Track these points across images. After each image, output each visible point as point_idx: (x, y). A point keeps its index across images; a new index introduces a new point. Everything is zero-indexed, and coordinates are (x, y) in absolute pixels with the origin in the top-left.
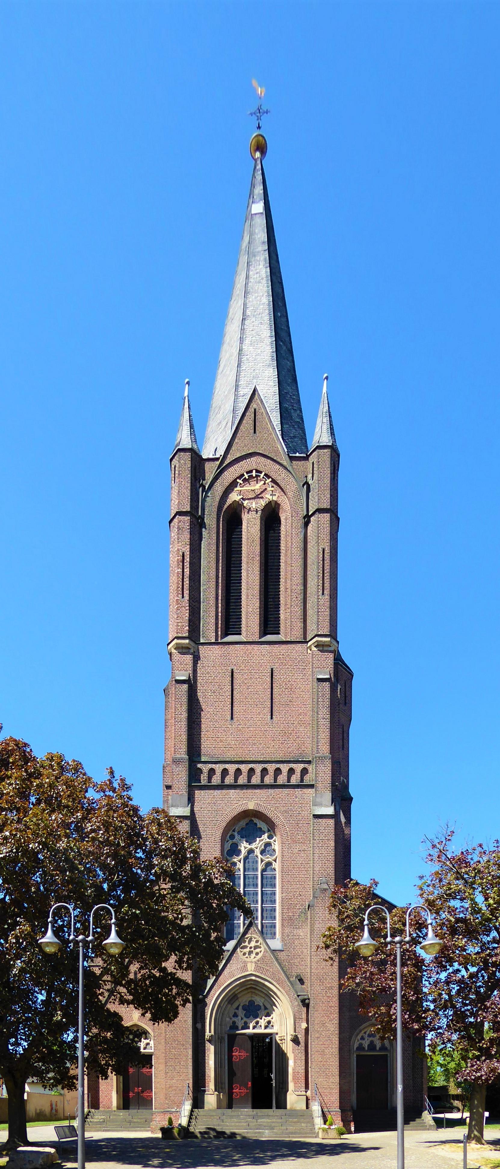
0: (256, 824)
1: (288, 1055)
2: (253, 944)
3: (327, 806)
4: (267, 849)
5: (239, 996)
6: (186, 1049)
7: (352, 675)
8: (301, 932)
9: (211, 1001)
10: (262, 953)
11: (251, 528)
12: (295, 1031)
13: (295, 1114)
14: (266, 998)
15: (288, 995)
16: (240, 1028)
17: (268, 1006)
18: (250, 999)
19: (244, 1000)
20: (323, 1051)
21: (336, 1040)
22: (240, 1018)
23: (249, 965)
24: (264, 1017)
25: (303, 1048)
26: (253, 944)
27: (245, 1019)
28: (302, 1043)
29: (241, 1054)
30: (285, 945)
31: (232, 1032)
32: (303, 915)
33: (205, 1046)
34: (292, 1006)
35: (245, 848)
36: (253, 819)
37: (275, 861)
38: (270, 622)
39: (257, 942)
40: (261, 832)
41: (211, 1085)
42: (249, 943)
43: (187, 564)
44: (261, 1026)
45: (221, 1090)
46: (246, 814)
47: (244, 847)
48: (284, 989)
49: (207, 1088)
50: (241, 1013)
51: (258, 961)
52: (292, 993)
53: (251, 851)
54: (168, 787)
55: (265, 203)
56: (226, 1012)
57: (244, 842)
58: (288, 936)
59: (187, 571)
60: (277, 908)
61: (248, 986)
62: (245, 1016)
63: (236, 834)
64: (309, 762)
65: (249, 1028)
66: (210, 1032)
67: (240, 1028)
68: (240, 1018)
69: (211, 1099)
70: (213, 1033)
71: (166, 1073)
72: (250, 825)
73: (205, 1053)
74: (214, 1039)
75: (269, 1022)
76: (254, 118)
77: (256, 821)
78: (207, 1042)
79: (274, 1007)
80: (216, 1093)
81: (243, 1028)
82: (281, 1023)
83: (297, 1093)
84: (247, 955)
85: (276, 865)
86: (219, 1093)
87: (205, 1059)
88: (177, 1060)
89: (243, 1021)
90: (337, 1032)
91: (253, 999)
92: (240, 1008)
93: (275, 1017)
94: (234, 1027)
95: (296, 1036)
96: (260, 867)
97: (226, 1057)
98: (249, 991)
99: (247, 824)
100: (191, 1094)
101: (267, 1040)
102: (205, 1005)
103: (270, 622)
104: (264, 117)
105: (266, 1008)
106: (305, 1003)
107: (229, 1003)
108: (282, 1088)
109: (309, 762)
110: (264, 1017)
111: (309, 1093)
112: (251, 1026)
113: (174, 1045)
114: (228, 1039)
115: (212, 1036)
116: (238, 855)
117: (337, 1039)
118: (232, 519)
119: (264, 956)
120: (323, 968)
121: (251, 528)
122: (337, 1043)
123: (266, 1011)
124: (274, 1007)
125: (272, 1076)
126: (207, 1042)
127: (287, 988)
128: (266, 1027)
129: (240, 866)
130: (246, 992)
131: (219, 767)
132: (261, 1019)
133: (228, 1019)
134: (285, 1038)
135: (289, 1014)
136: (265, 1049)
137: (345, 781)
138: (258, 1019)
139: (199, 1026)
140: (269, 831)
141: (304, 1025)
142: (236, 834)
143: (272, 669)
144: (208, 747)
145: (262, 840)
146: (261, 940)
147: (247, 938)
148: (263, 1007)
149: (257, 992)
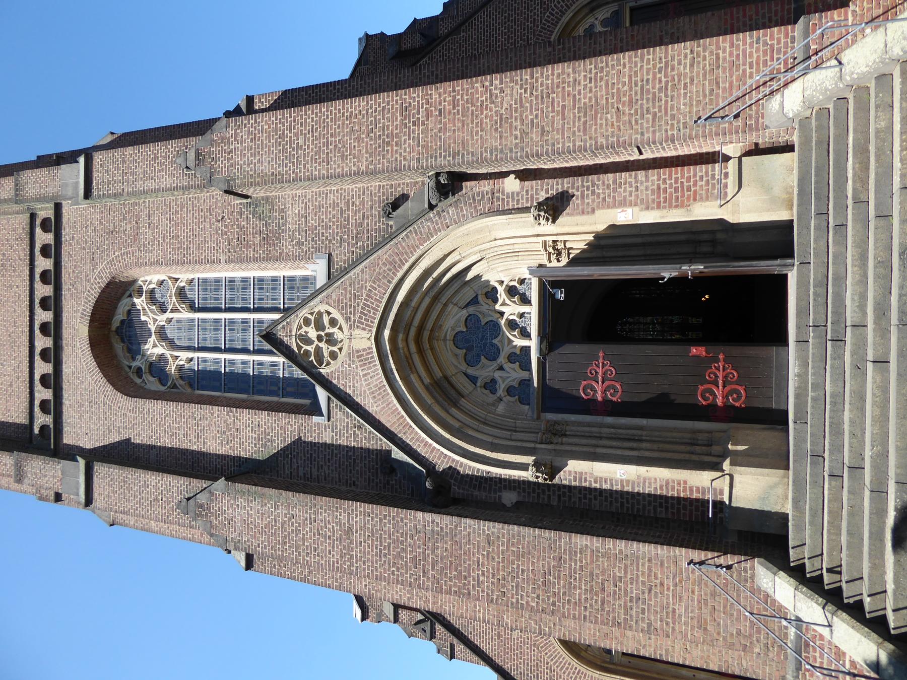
0: (122, 322)
1: (601, 227)
2: (313, 333)
5: (439, 374)
6: (572, 553)
8: (292, 213)
9: (443, 458)
10: (331, 309)
12: (526, 210)
13: (816, 187)
14: (444, 300)
15: (437, 231)
16: (524, 375)
17: (467, 294)
18: (450, 344)
19: (451, 360)
20: (585, 110)
21: (549, 76)
22: (497, 375)
24: (498, 307)
25: (579, 181)
26: (313, 333)
27: (502, 359)
28: (566, 184)
29: (601, 375)
30: (318, 250)
31: (534, 399)
32: (259, 210)
33: (570, 488)
34: (458, 223)
35: (155, 346)
36: (114, 328)
39: (307, 322)
40: (132, 311)
41: (698, 482)
42: (309, 341)
44: (522, 315)
45: (716, 449)
47: (153, 349)
48: (414, 248)
49: (710, 497)
50: (485, 371)
51: (348, 319)
52: (425, 225)
53: (162, 333)
54: (58, 497)
56: (482, 413)
57: (146, 347)
58: (300, 244)
60: (289, 273)
61: (413, 348)
64: (33, 216)
65: (527, 349)
66: (523, 467)
67: (524, 375)
68: (497, 375)
69: (750, 488)
70: (529, 460)
73: (590, 490)
74: (548, 458)
75: (511, 291)
78: (556, 481)
79: (470, 275)
80: (726, 465)
81: (527, 367)
82: (509, 251)
83: (731, 189)
84: (335, 349)
85: (184, 276)
86: (724, 457)
87: (611, 492)
88: (610, 589)
89: (508, 366)
90: (526, 74)
91: (450, 336)
92: (471, 371)
93: (496, 274)
94: (521, 390)
95: (540, 206)
96: (186, 315)
97: (609, 420)
98: (426, 346)
99: (123, 341)
100: (730, 559)
101: (560, 295)
102: (452, 472)
105: (474, 301)
106: (450, 184)
107: (455, 404)
108: (713, 242)
109: (33, 216)
110: (498, 307)
111: (732, 149)
112: (520, 342)
113: (559, 587)
114: (557, 415)
115: (537, 464)
116: (166, 360)
117: (548, 70)
119: (338, 304)
120: (358, 140)
122: (558, 68)
123: (481, 299)
124: (470, 275)
125: (667, 275)
126: (556, 481)
127: (413, 239)
128: (525, 300)
129: (184, 355)
130: (429, 353)
131: (39, 392)
132: (502, 314)
133: (501, 408)
134: (549, 239)
135: (479, 231)
136: (585, 307)
138: (503, 322)
139: (509, 498)
141: (511, 184)
142: (134, 364)
145: (144, 309)
146: (304, 313)
147: (299, 348)
148: (472, 309)
149: (430, 325)
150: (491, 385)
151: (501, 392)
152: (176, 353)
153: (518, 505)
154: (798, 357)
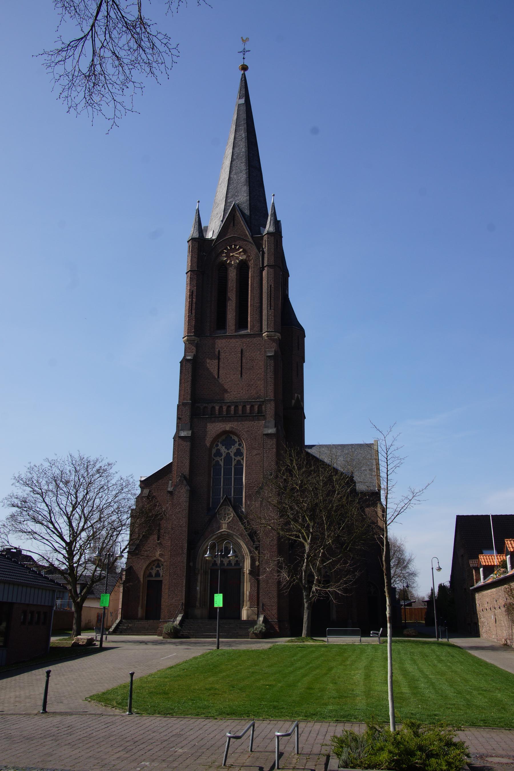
0: (231, 437)
3: (248, 616)
4: (239, 453)
11: (232, 274)
37: (221, 460)
38: (242, 323)
40: (234, 442)
43: (194, 297)
46: (225, 432)
51: (229, 522)
55: (245, 98)
59: (194, 300)
63: (219, 444)
71: (169, 595)
72: (227, 438)
76: (242, 54)
103: (242, 323)
104: (247, 54)
118: (224, 267)
121: (232, 274)
129: (222, 463)
137: (299, 396)
139: (191, 564)
140: (239, 441)
142: (219, 444)
143: (242, 350)
144: (217, 361)
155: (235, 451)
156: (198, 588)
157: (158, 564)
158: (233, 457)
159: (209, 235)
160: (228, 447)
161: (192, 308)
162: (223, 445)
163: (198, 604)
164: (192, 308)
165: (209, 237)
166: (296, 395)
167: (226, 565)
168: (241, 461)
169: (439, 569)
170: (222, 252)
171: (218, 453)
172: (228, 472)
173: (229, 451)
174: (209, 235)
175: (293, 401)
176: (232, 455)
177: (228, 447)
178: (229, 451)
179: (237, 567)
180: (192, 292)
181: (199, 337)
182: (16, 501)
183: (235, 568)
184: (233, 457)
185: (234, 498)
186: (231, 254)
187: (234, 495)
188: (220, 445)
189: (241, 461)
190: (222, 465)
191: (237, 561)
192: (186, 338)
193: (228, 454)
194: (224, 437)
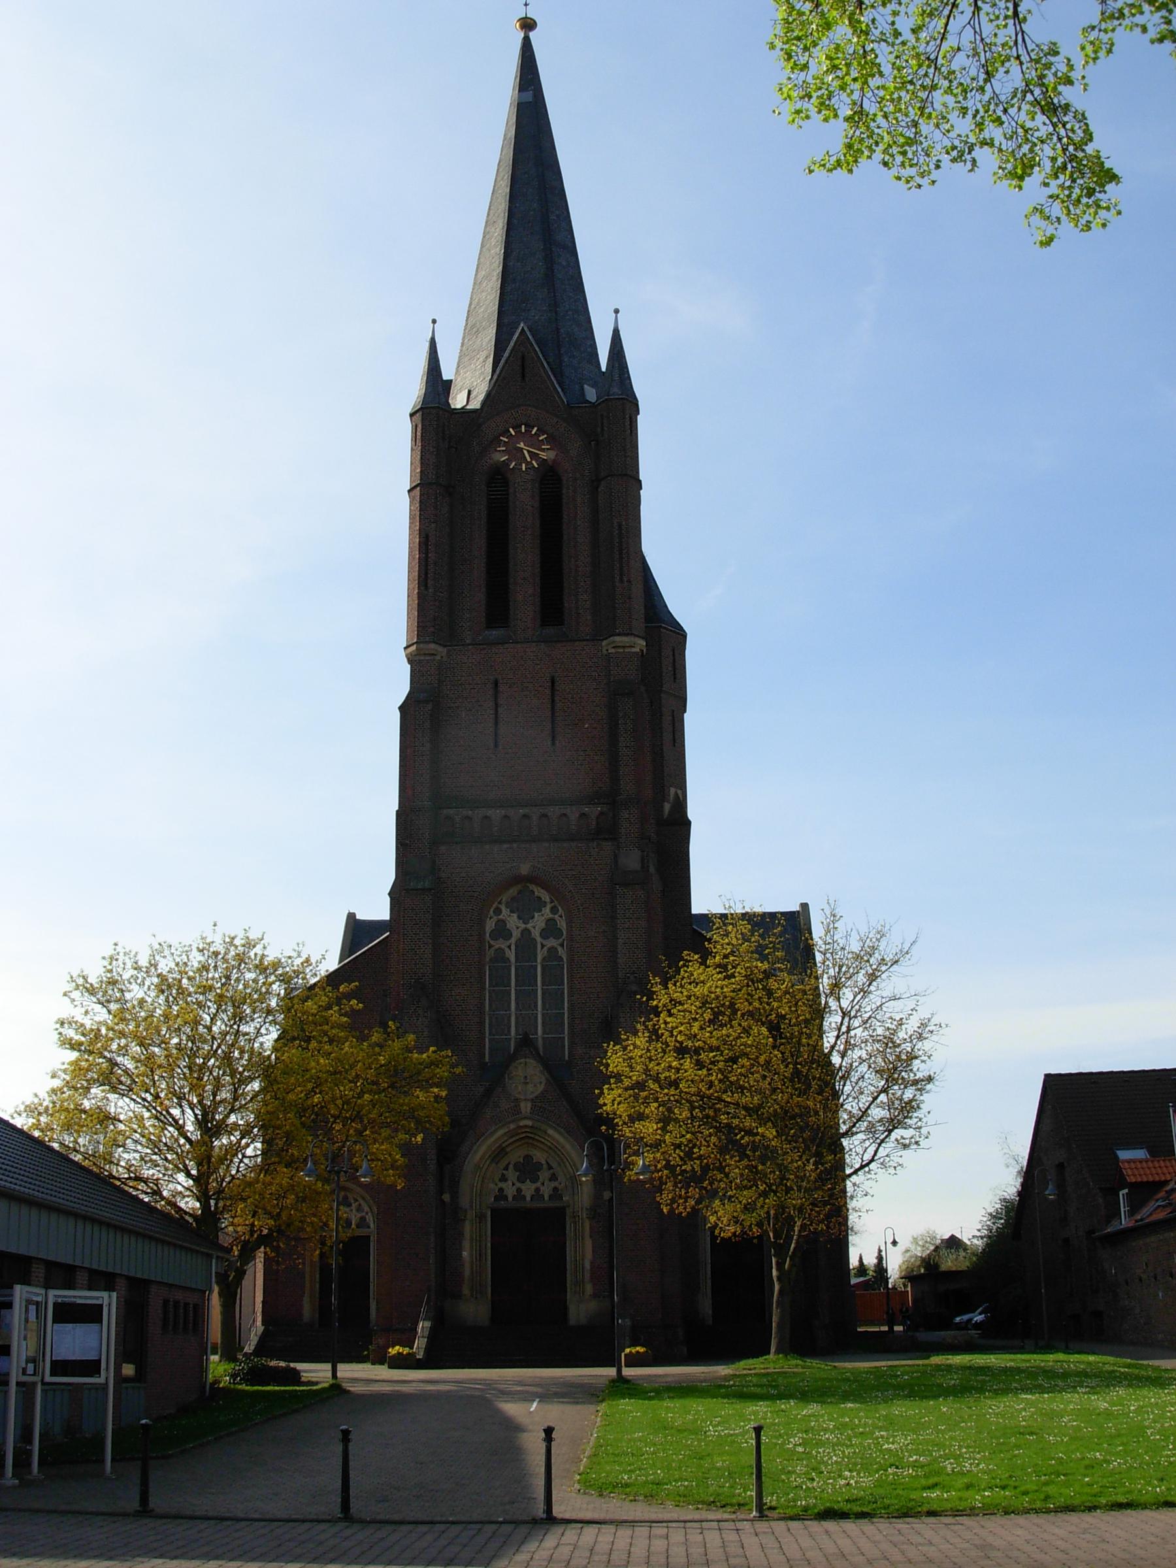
5: (508, 1149)
7: (683, 635)
19: (517, 1156)
23: (522, 1105)
27: (518, 1185)
37: (509, 947)
50: (512, 1175)
62: (518, 1180)
63: (503, 907)
77: (532, 887)
92: (511, 1166)
103: (552, 610)
121: (525, 503)
129: (511, 955)
133: (492, 1186)
137: (679, 792)
140: (552, 902)
148: (545, 1166)
150: (504, 1179)
151: (501, 1185)
152: (513, 947)
153: (443, 1202)
154: (555, 1382)
155: (543, 925)
156: (465, 1254)
157: (346, 1198)
158: (539, 939)
159: (458, 400)
160: (525, 917)
161: (426, 574)
162: (512, 912)
163: (466, 1291)
164: (426, 574)
165: (459, 406)
166: (672, 790)
167: (528, 1198)
168: (507, 950)
169: (894, 1243)
170: (496, 441)
171: (502, 931)
172: (527, 977)
173: (529, 926)
174: (458, 400)
175: (667, 807)
176: (536, 934)
177: (525, 917)
178: (529, 926)
179: (557, 1204)
180: (427, 537)
181: (445, 646)
182: (71, 1033)
183: (551, 1205)
184: (539, 939)
185: (543, 1038)
186: (522, 445)
187: (544, 1032)
188: (505, 911)
189: (507, 950)
190: (513, 959)
191: (555, 1189)
192: (414, 648)
193: (526, 932)
194: (513, 891)
